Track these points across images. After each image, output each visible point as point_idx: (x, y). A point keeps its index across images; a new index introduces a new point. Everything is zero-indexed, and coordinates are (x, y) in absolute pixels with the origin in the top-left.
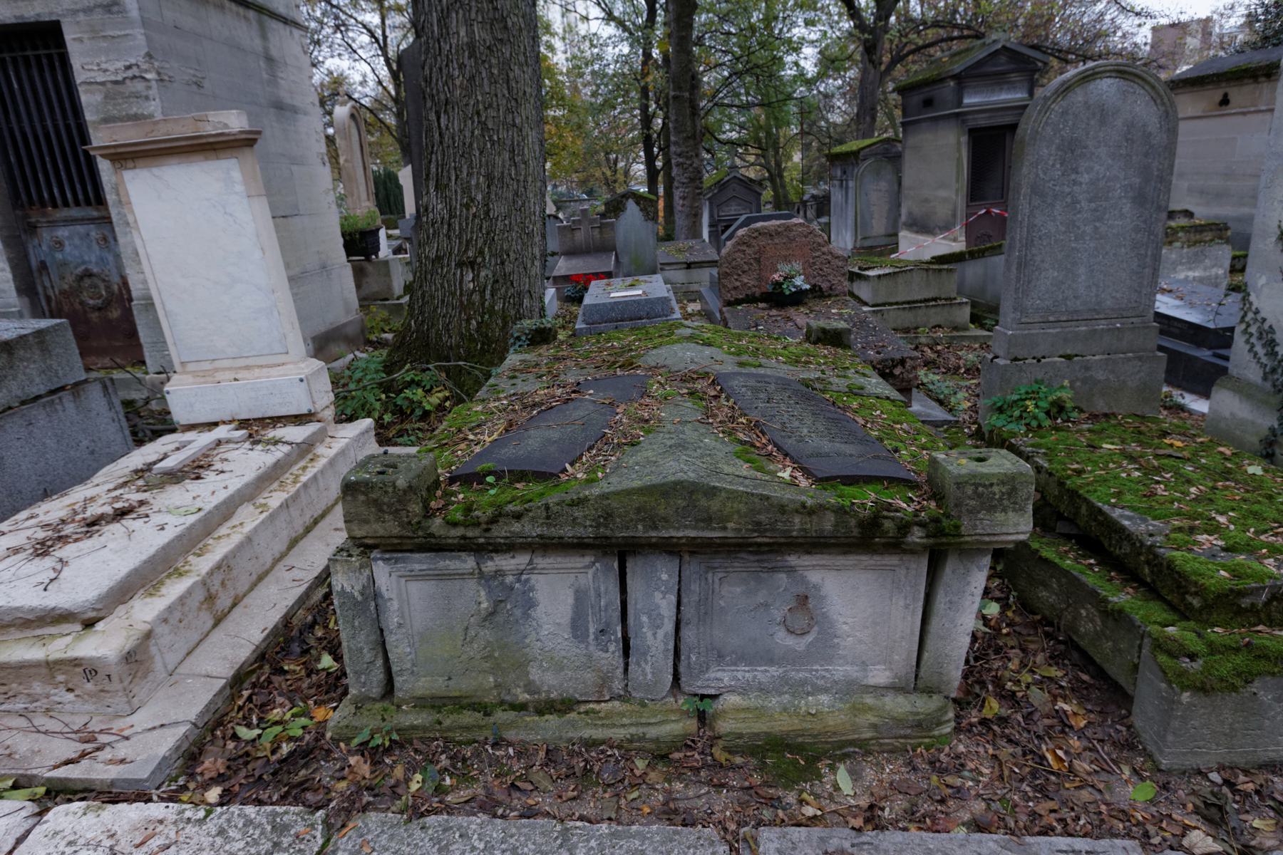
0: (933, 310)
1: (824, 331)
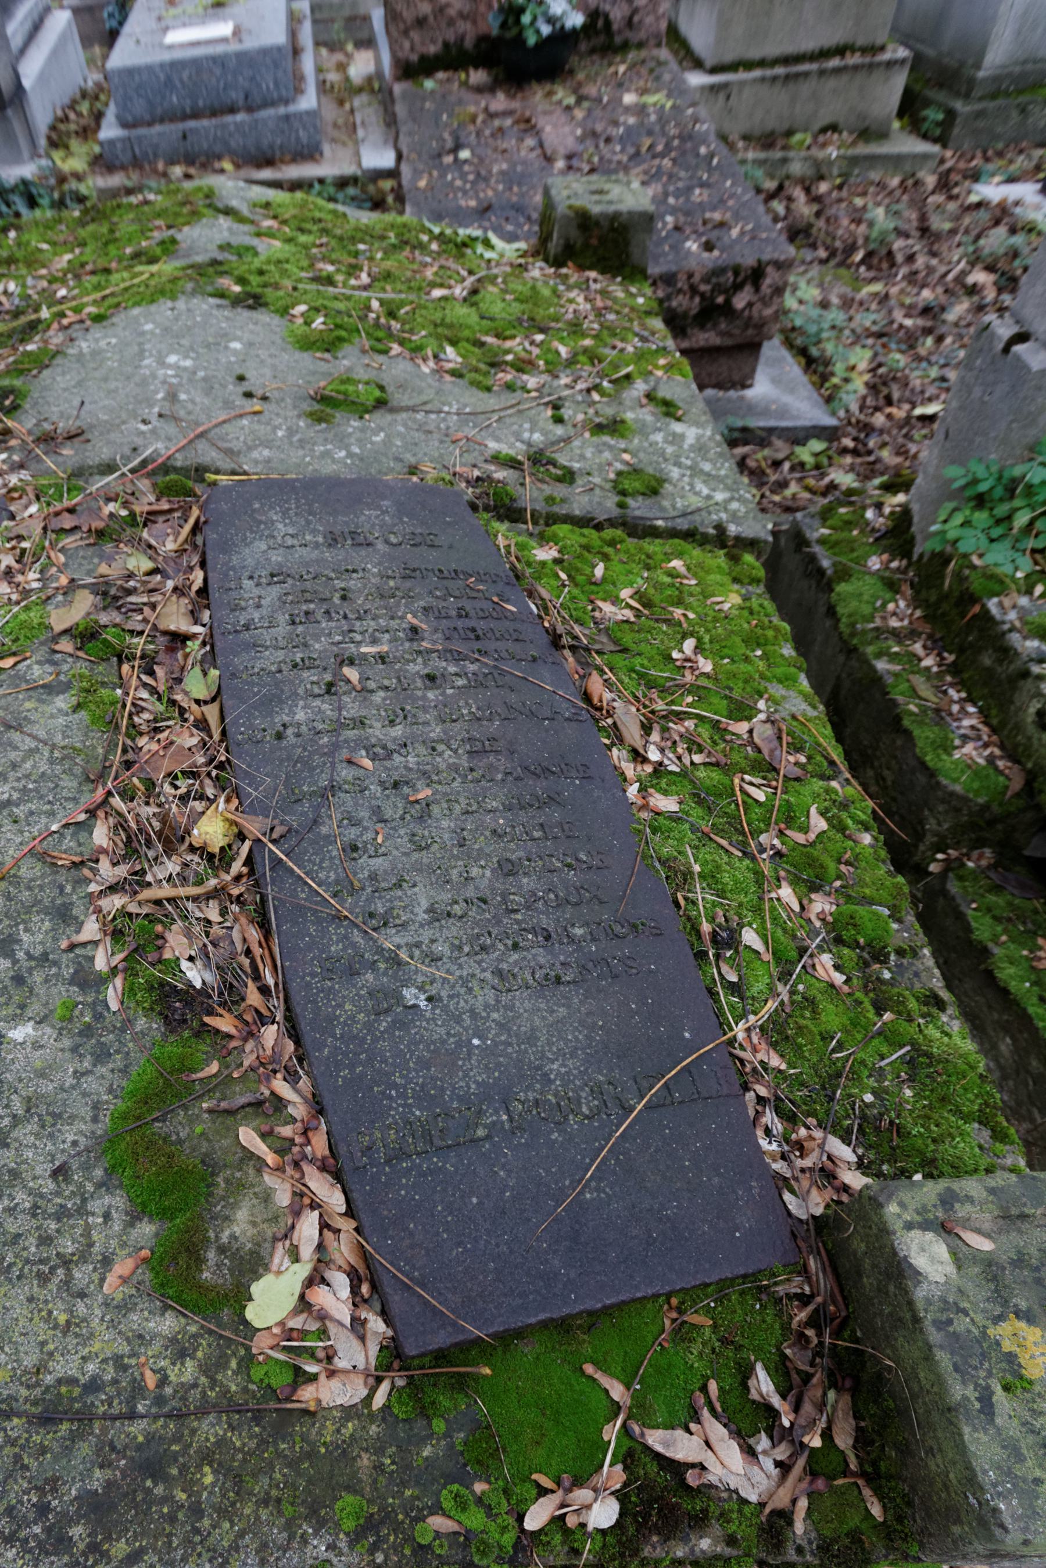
0: (832, 83)
1: (584, 220)
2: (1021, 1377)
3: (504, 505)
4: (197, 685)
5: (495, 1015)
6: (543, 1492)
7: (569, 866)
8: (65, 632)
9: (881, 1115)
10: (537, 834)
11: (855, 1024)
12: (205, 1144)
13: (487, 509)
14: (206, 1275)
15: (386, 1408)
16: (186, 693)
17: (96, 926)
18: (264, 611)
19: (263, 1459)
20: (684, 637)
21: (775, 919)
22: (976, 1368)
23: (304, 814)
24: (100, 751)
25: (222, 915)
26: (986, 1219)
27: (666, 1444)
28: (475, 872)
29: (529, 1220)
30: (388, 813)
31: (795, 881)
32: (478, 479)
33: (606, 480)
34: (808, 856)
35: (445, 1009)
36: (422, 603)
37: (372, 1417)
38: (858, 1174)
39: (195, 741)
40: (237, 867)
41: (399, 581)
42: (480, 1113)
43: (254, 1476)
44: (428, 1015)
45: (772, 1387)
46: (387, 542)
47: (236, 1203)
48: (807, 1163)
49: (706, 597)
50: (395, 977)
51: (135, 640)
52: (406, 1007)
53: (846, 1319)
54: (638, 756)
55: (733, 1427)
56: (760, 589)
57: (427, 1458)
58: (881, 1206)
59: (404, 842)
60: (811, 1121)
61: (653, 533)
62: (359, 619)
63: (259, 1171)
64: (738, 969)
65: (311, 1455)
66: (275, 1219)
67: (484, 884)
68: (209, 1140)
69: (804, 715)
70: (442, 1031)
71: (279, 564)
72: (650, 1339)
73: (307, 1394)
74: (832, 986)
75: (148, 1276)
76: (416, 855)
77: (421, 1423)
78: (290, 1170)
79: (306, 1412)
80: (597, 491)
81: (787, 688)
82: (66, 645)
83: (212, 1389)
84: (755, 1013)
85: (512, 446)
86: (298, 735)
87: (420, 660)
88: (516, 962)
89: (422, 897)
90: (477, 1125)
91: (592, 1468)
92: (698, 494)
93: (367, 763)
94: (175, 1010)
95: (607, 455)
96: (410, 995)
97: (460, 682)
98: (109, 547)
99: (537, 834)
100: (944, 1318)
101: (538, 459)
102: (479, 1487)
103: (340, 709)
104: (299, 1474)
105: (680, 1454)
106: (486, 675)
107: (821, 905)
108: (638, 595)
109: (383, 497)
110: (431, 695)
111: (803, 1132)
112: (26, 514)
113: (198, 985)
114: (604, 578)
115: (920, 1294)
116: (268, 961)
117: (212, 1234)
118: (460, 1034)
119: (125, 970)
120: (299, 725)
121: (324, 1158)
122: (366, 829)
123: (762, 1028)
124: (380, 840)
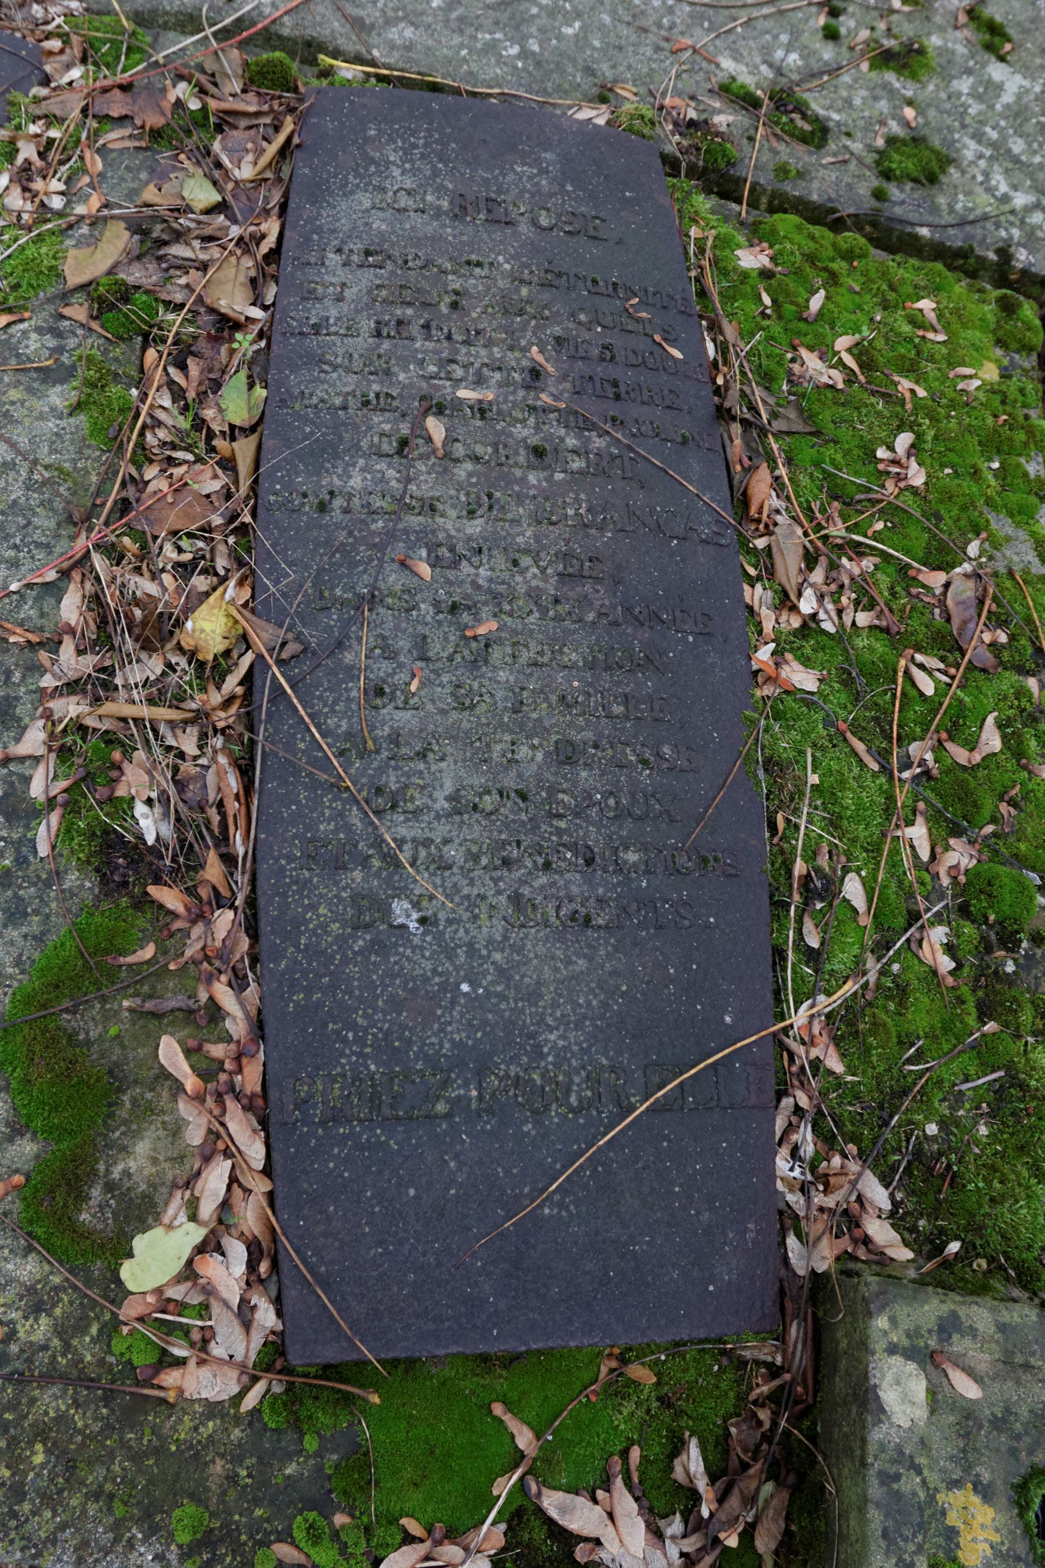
2: (954, 1560)
3: (716, 170)
4: (236, 403)
5: (497, 956)
6: (409, 1539)
7: (645, 763)
8: (83, 287)
9: (940, 1154)
10: (618, 709)
11: (946, 1029)
12: (118, 1051)
13: (693, 172)
14: (84, 1216)
15: (256, 1412)
16: (221, 411)
17: (42, 736)
18: (345, 307)
19: (104, 1447)
20: (900, 429)
21: (894, 864)
22: (906, 1540)
23: (329, 629)
24: (94, 479)
25: (200, 747)
26: (983, 1360)
27: (563, 1510)
28: (523, 752)
29: (468, 1229)
30: (435, 648)
31: (935, 819)
32: (692, 123)
33: (871, 149)
34: (962, 784)
35: (439, 936)
36: (557, 330)
37: (237, 1419)
38: (886, 1225)
39: (215, 486)
40: (232, 683)
41: (535, 288)
42: (446, 1083)
43: (90, 1463)
44: (416, 940)
45: (701, 1469)
46: (534, 222)
47: (140, 1131)
48: (830, 1201)
49: (952, 365)
50: (388, 883)
51: (170, 317)
52: (391, 926)
53: (809, 1409)
54: (785, 602)
55: (646, 1503)
56: (1029, 362)
57: (289, 1477)
58: (870, 1315)
59: (443, 693)
60: (852, 1148)
61: (810, 434)
62: (466, 342)
63: (174, 1098)
64: (824, 928)
65: (159, 1452)
66: (180, 1159)
67: (531, 770)
68: (123, 1047)
69: (1026, 572)
70: (428, 965)
71: (381, 234)
72: (578, 1386)
73: (170, 1378)
74: (935, 973)
75: (18, 1206)
76: (455, 715)
77: (291, 1435)
78: (210, 1101)
79: (164, 1401)
80: (853, 166)
81: (1018, 525)
82: (78, 311)
83: (64, 1355)
84: (829, 994)
85: (754, 70)
86: (346, 511)
87: (532, 421)
88: (542, 887)
89: (448, 776)
90: (438, 1098)
91: (470, 1523)
92: (990, 190)
93: (425, 570)
94: (117, 867)
95: (883, 105)
96: (402, 911)
97: (577, 464)
98: (164, 156)
99: (618, 709)
100: (892, 1470)
101: (784, 100)
102: (340, 1519)
103: (408, 480)
104: (140, 1471)
105: (574, 1524)
106: (613, 458)
107: (960, 856)
108: (859, 351)
109: (547, 146)
110: (532, 478)
111: (837, 1161)
112: (66, 79)
113: (150, 840)
114: (820, 314)
115: (876, 1435)
116: (242, 822)
117: (101, 1167)
118: (446, 974)
119: (65, 805)
120: (350, 496)
121: (254, 1095)
122: (401, 665)
123: (829, 1016)
124: (413, 688)
